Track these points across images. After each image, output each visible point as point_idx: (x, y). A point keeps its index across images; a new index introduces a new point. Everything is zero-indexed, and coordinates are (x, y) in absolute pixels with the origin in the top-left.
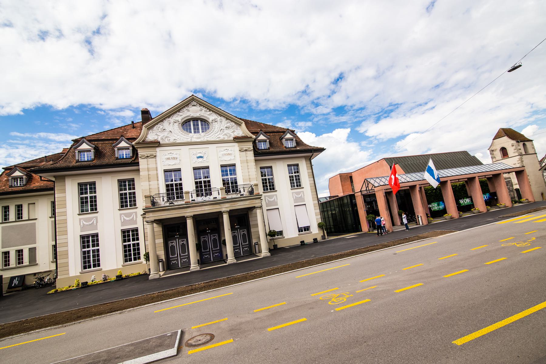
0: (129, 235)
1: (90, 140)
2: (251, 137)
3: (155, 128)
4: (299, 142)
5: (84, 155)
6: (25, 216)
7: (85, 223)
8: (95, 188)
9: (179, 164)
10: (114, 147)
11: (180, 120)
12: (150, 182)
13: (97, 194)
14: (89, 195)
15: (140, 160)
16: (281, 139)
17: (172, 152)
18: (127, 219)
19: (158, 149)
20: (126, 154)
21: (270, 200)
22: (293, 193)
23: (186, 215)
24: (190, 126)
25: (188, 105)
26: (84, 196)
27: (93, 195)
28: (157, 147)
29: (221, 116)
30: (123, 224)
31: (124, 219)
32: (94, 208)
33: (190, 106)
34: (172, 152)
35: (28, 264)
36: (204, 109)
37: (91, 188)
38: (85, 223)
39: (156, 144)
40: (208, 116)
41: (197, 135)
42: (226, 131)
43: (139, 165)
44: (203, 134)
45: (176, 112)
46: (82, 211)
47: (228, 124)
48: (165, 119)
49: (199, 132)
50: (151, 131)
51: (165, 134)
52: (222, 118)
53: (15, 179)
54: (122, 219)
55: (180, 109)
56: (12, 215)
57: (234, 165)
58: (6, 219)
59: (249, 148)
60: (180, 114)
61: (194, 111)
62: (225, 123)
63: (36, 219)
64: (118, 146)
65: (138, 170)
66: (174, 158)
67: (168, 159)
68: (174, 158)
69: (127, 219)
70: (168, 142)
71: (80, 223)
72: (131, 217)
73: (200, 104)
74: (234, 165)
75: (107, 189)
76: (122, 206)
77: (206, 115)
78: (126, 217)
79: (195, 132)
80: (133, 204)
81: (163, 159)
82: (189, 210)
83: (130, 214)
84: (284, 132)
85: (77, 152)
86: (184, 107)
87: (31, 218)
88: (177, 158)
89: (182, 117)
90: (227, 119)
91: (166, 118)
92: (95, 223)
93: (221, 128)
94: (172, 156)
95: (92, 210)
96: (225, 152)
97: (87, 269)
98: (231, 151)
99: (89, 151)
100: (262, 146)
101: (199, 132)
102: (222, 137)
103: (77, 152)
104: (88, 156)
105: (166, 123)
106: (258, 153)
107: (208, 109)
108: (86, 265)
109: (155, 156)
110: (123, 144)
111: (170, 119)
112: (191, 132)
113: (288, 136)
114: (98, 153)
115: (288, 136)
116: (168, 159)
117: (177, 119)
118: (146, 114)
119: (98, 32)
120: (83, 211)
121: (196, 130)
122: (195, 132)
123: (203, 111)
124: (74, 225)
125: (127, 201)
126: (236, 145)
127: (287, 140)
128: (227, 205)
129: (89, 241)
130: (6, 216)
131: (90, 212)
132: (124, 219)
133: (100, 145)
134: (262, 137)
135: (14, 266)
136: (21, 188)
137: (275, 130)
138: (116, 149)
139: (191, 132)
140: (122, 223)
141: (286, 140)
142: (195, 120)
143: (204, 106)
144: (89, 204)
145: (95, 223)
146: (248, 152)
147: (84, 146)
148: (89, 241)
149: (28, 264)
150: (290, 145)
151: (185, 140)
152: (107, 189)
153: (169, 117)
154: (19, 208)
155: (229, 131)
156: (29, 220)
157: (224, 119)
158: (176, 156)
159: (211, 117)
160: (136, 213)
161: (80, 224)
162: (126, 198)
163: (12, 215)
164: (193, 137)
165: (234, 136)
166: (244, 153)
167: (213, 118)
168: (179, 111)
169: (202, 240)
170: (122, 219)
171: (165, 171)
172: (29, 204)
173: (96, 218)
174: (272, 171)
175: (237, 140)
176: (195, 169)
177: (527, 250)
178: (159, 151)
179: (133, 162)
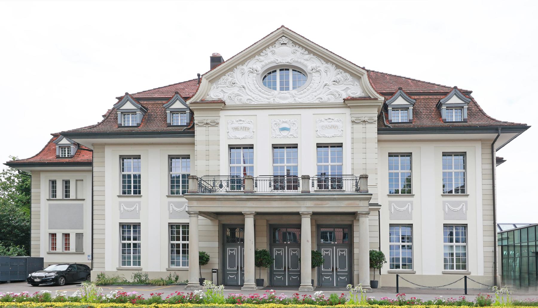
0: (178, 232)
1: (137, 99)
2: (376, 99)
3: (221, 81)
4: (475, 110)
6: (72, 195)
7: (175, 208)
9: (251, 138)
10: (166, 109)
11: (259, 69)
12: (211, 159)
15: (196, 128)
16: (439, 106)
17: (242, 118)
18: (177, 209)
19: (222, 113)
20: (181, 120)
23: (301, 210)
24: (275, 78)
25: (274, 43)
28: (221, 109)
29: (327, 61)
30: (171, 215)
31: (173, 209)
33: (277, 44)
34: (242, 118)
35: (74, 251)
36: (300, 50)
38: (175, 208)
39: (219, 105)
40: (306, 62)
41: (285, 93)
42: (333, 88)
43: (194, 136)
44: (294, 92)
45: (253, 56)
46: (172, 193)
47: (339, 76)
48: (235, 66)
49: (287, 89)
50: (214, 85)
51: (235, 90)
52: (329, 65)
53: (62, 148)
54: (171, 209)
55: (261, 51)
56: (60, 193)
58: (66, 196)
59: (371, 118)
60: (262, 58)
61: (285, 54)
62: (333, 73)
63: (84, 200)
64: (172, 107)
65: (193, 144)
66: (246, 129)
67: (236, 129)
68: (246, 129)
69: (177, 209)
70: (238, 103)
71: (120, 207)
73: (293, 42)
75: (154, 169)
76: (124, 193)
77: (302, 61)
78: (176, 206)
79: (282, 89)
81: (228, 129)
82: (249, 204)
83: (458, 204)
84: (446, 94)
85: (119, 113)
86: (268, 47)
87: (78, 198)
88: (249, 129)
89: (263, 63)
90: (338, 67)
91: (238, 64)
92: (137, 209)
93: (324, 84)
94: (242, 125)
96: (326, 123)
97: (126, 266)
98: (338, 121)
99: (134, 113)
100: (397, 117)
101: (287, 89)
102: (326, 98)
103: (119, 113)
104: (131, 121)
105: (237, 72)
106: (385, 127)
107: (306, 49)
108: (125, 261)
109: (218, 124)
110: (178, 105)
111: (244, 67)
112: (275, 89)
113: (454, 100)
114: (147, 116)
115: (454, 100)
116: (236, 129)
117: (255, 67)
118: (216, 60)
120: (125, 192)
121: (284, 87)
122: (282, 89)
123: (298, 53)
124: (114, 209)
126: (347, 111)
127: (450, 108)
128: (309, 204)
129: (130, 230)
130: (66, 192)
131: (132, 194)
132: (173, 209)
133: (149, 105)
134: (400, 101)
135: (61, 251)
136: (67, 160)
137: (436, 90)
138: (168, 112)
139: (275, 89)
140: (170, 214)
141: (448, 108)
142: (284, 68)
143: (300, 45)
144: (131, 186)
145: (137, 209)
146: (368, 126)
147: (129, 106)
148: (130, 230)
149: (74, 251)
150: (454, 117)
151: (265, 101)
152: (154, 169)
153: (243, 63)
154: (67, 183)
155: (339, 89)
156: (76, 200)
157: (332, 68)
158: (247, 125)
159: (309, 63)
162: (129, 182)
163: (60, 193)
164: (277, 96)
165: (345, 97)
166: (360, 126)
167: (314, 65)
168: (259, 53)
169: (229, 252)
170: (171, 209)
172: (77, 180)
175: (349, 102)
176: (275, 147)
178: (224, 117)
179: (189, 131)
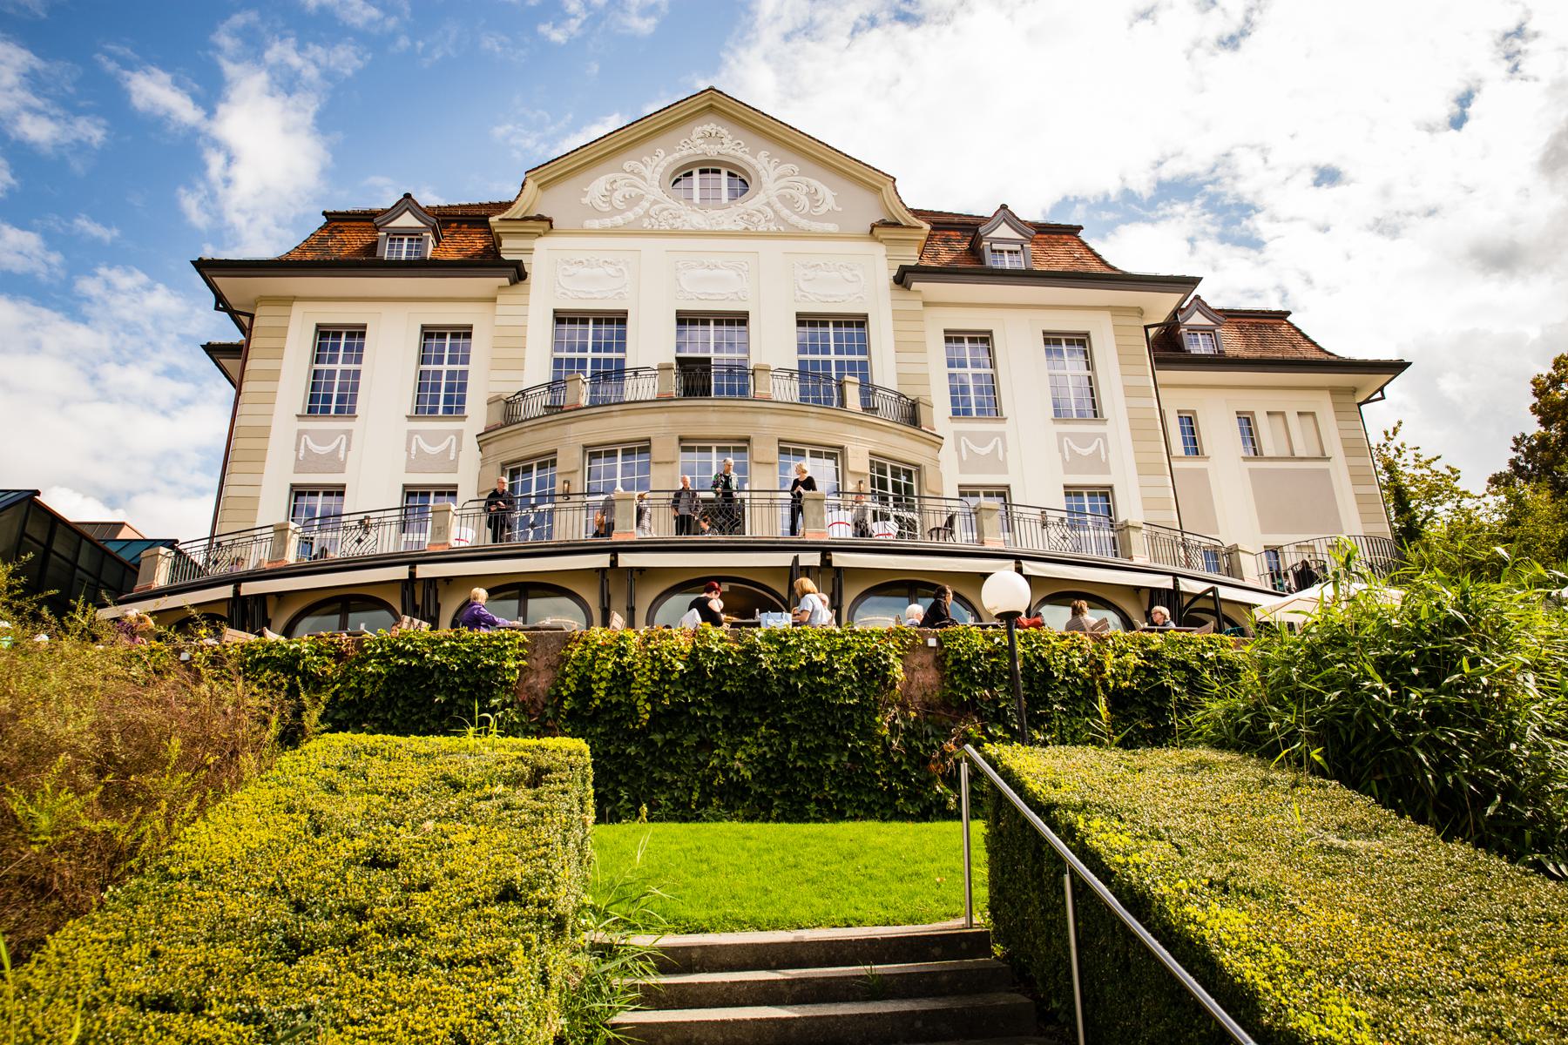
5: (409, 253)
7: (312, 445)
8: (361, 348)
13: (364, 368)
14: (339, 366)
21: (977, 450)
22: (1060, 436)
26: (432, 367)
27: (352, 367)
31: (970, 451)
32: (346, 407)
37: (348, 347)
57: (861, 322)
64: (392, 224)
72: (334, 446)
74: (861, 322)
80: (456, 407)
95: (448, 410)
119: (1515, 68)
125: (438, 397)
132: (970, 451)
142: (709, 168)
160: (459, 434)
161: (408, 449)
171: (561, 318)
173: (349, 433)
174: (622, 336)
177: (790, 983)
